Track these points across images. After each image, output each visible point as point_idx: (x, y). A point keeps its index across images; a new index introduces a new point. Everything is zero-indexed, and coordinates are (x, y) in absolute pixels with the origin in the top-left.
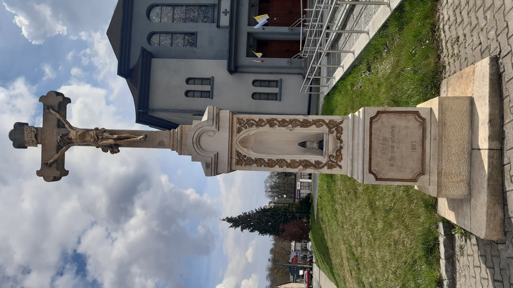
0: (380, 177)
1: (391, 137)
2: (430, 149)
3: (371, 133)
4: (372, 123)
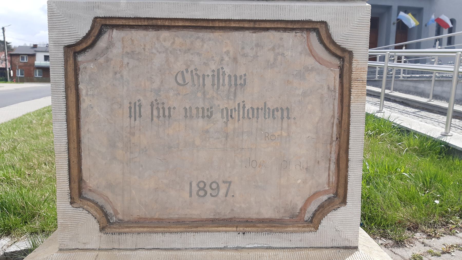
0: (81, 67)
1: (248, 107)
2: (202, 249)
3: (263, 25)
4: (302, 30)
